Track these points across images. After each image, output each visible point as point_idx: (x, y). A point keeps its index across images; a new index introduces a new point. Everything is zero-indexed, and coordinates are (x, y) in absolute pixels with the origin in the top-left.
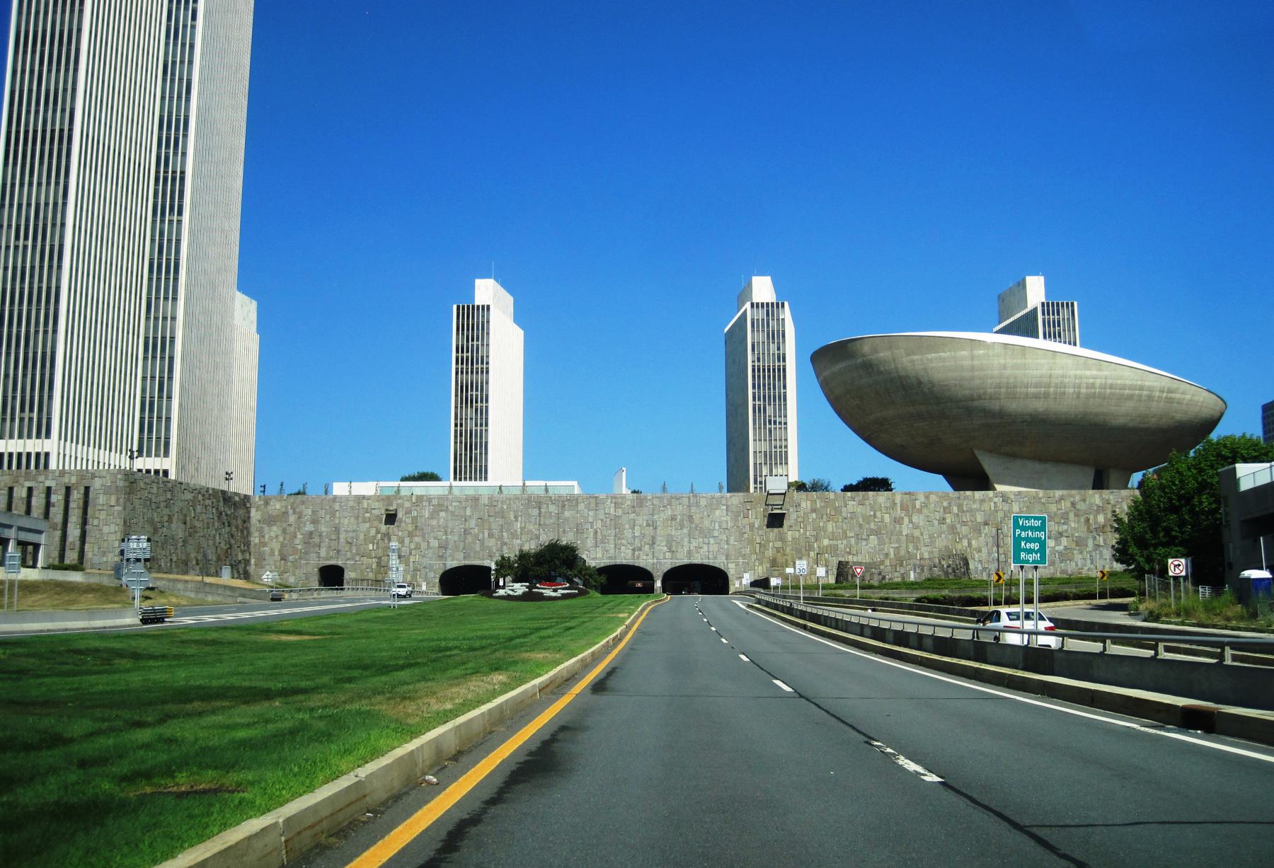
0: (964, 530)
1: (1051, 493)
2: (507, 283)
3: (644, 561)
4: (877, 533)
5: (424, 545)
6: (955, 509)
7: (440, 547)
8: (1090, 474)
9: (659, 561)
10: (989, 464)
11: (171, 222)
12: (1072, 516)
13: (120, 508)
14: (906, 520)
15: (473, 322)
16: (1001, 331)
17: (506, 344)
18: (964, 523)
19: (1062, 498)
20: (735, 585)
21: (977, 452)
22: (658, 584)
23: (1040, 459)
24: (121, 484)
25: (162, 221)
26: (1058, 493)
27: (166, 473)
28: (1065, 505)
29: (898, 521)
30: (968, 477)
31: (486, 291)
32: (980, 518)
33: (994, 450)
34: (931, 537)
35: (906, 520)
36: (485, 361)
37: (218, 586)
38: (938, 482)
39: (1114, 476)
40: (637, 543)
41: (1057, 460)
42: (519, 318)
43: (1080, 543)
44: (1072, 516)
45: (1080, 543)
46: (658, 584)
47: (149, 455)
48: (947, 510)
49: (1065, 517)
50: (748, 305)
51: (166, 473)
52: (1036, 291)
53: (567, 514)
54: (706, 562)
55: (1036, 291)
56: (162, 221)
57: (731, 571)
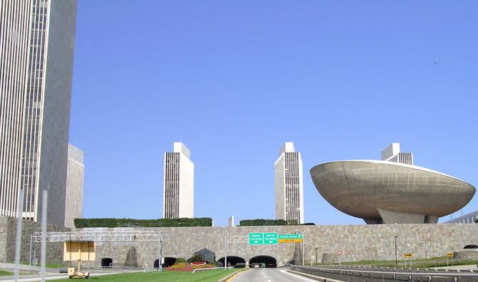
0: (374, 240)
1: (409, 225)
2: (187, 144)
3: (240, 254)
4: (338, 242)
5: (147, 249)
6: (370, 232)
7: (154, 250)
8: (423, 218)
9: (247, 255)
10: (383, 214)
11: (37, 72)
12: (417, 234)
13: (6, 234)
14: (350, 236)
15: (173, 158)
16: (390, 161)
17: (187, 168)
18: (374, 237)
19: (413, 227)
20: (280, 264)
21: (378, 209)
22: (247, 263)
23: (404, 212)
24: (6, 222)
25: (33, 71)
26: (411, 225)
27: (32, 219)
28: (414, 230)
29: (346, 236)
30: (374, 219)
31: (178, 147)
32: (380, 236)
33: (384, 208)
34: (360, 243)
35: (350, 236)
36: (178, 175)
37: (438, 266)
38: (361, 221)
39: (432, 218)
40: (238, 247)
41: (410, 212)
42: (192, 159)
43: (420, 245)
44: (417, 234)
45: (420, 245)
46: (247, 263)
47: (28, 211)
48: (367, 232)
49: (414, 234)
50: (284, 154)
51: (32, 219)
52: (396, 149)
53: (208, 235)
54: (267, 255)
55: (396, 149)
56: (33, 71)
57: (278, 258)
